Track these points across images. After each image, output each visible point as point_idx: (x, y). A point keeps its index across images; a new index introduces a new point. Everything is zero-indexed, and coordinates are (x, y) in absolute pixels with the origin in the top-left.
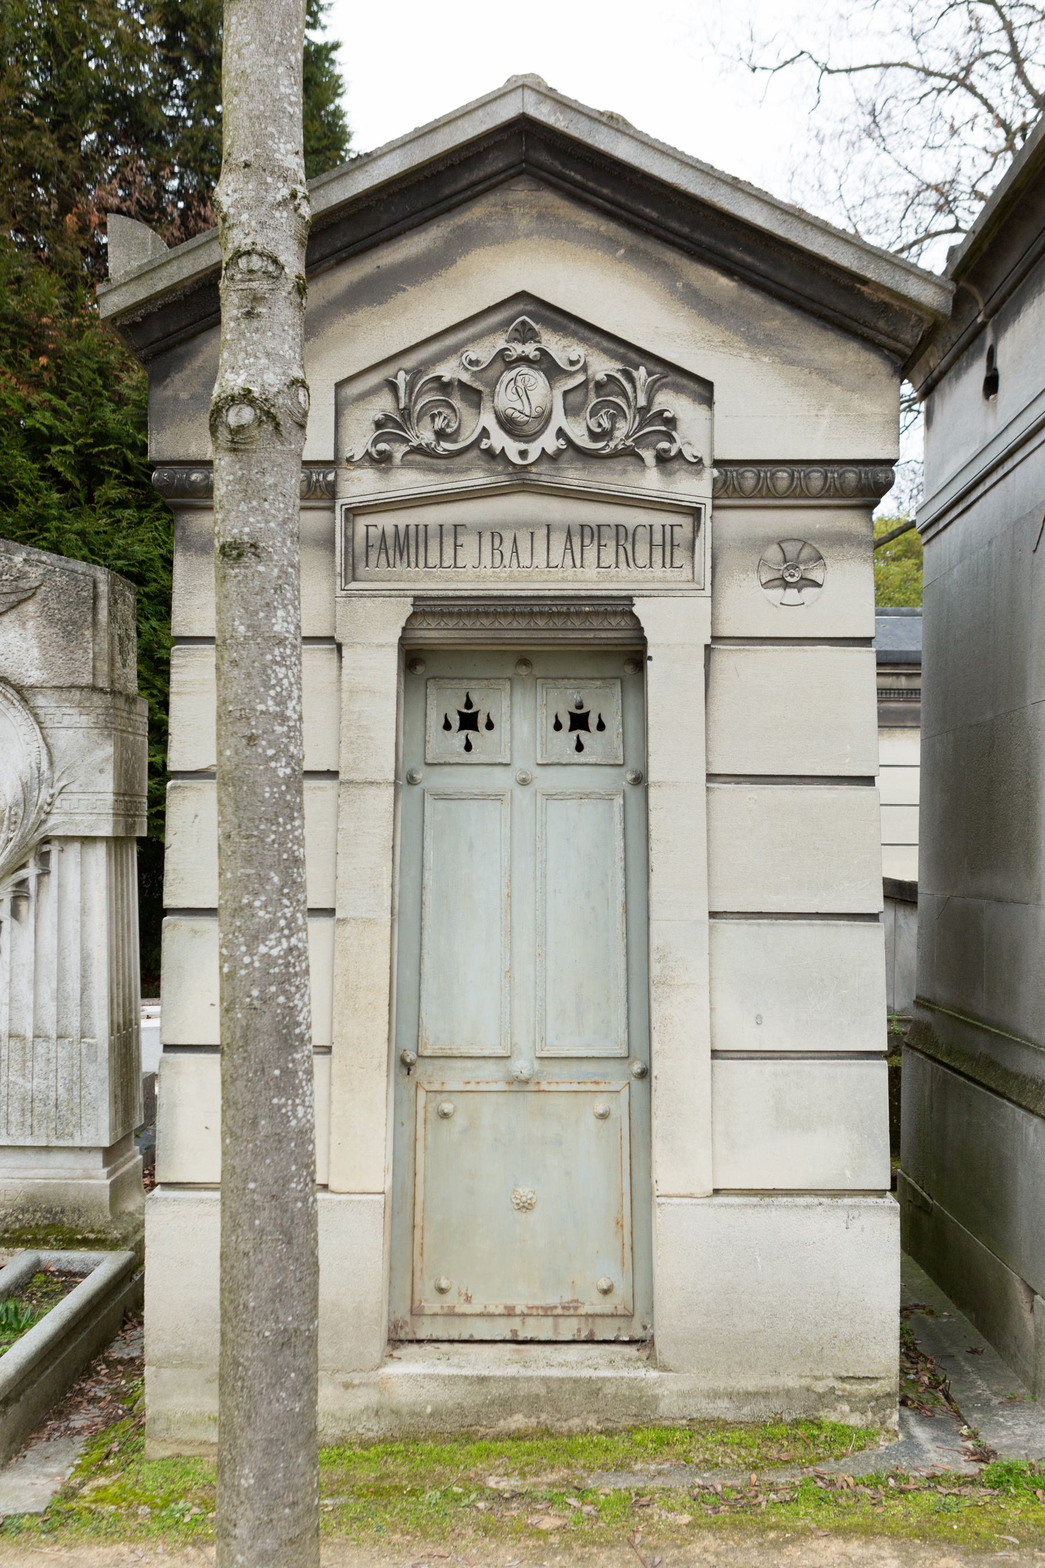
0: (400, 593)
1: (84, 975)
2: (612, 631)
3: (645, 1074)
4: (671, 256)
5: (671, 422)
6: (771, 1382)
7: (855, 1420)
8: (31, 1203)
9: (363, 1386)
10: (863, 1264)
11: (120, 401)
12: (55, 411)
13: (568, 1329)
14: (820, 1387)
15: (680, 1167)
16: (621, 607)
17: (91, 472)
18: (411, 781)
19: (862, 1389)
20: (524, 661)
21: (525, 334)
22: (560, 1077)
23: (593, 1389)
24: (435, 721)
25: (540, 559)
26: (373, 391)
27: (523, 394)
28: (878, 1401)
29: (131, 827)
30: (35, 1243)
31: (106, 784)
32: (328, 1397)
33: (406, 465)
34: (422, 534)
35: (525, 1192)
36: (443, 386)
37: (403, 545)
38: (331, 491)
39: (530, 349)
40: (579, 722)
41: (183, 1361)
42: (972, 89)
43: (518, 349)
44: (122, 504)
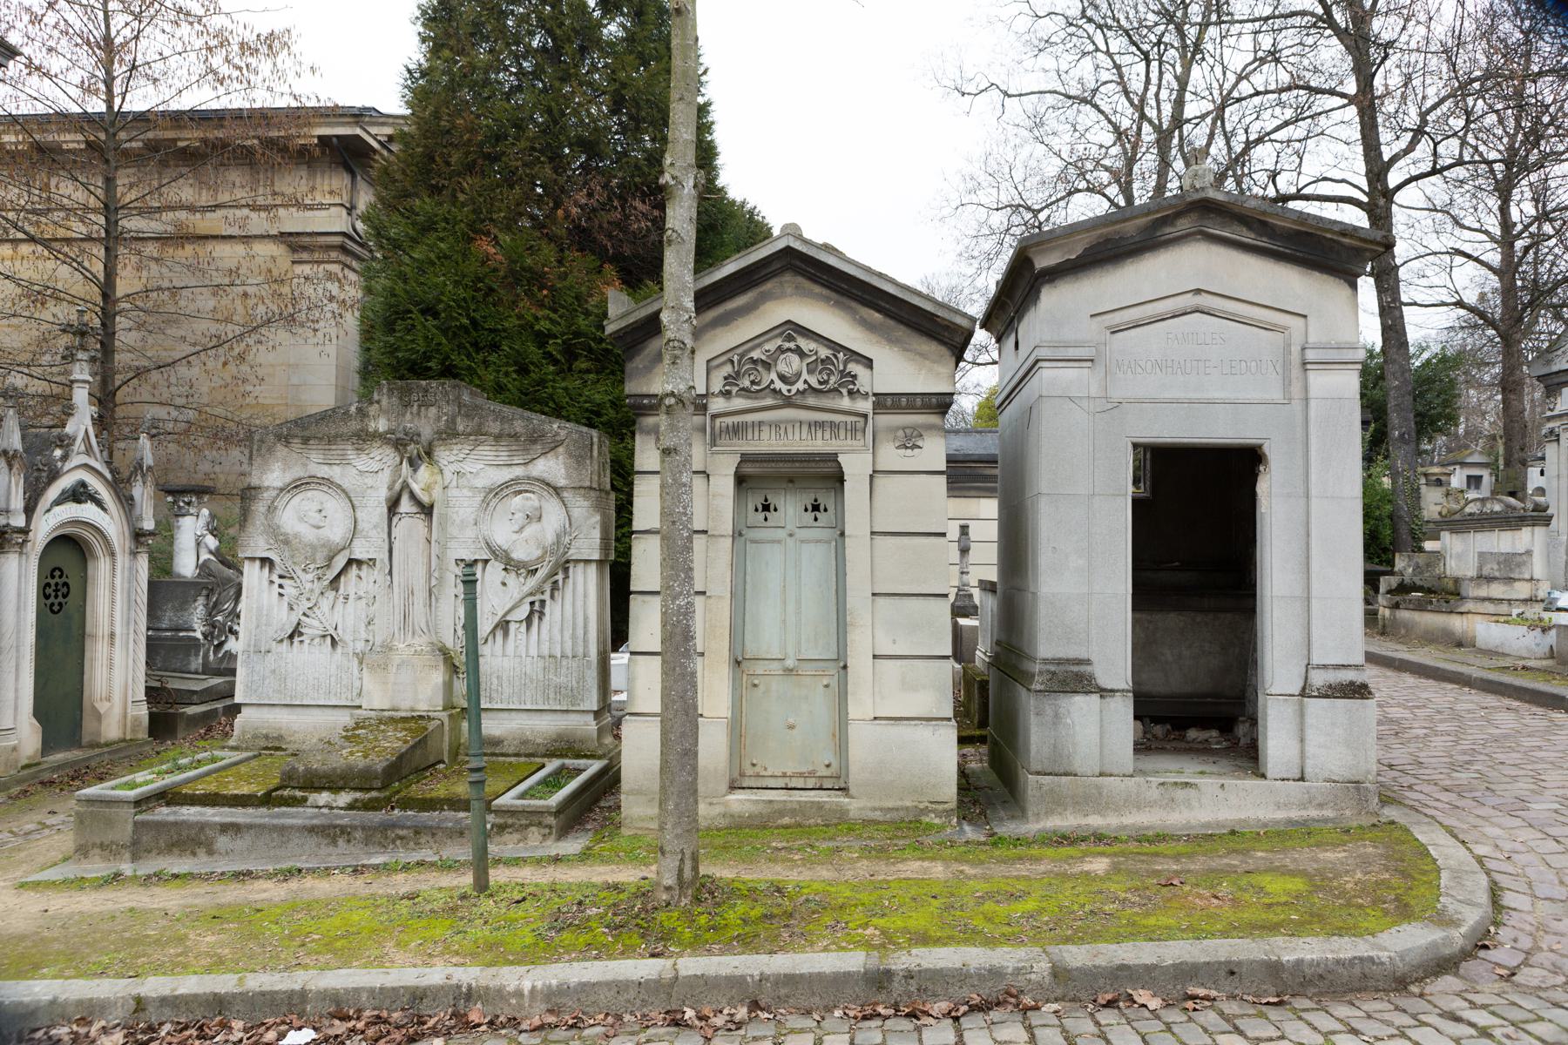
0: (735, 452)
1: (585, 627)
2: (828, 468)
3: (845, 667)
4: (854, 304)
5: (855, 377)
6: (899, 803)
7: (937, 821)
8: (560, 737)
9: (720, 804)
10: (939, 755)
11: (587, 313)
12: (552, 321)
13: (811, 783)
14: (921, 806)
15: (859, 707)
16: (833, 458)
17: (570, 353)
18: (740, 534)
19: (941, 807)
20: (791, 481)
21: (790, 338)
22: (808, 669)
23: (820, 806)
24: (751, 507)
25: (797, 437)
26: (723, 364)
27: (789, 365)
28: (948, 813)
29: (607, 555)
30: (561, 756)
31: (596, 534)
32: (703, 809)
33: (737, 395)
34: (745, 426)
35: (791, 720)
36: (754, 362)
37: (736, 431)
38: (705, 407)
39: (792, 345)
40: (816, 508)
41: (638, 792)
42: (1096, 107)
43: (787, 345)
44: (588, 371)
